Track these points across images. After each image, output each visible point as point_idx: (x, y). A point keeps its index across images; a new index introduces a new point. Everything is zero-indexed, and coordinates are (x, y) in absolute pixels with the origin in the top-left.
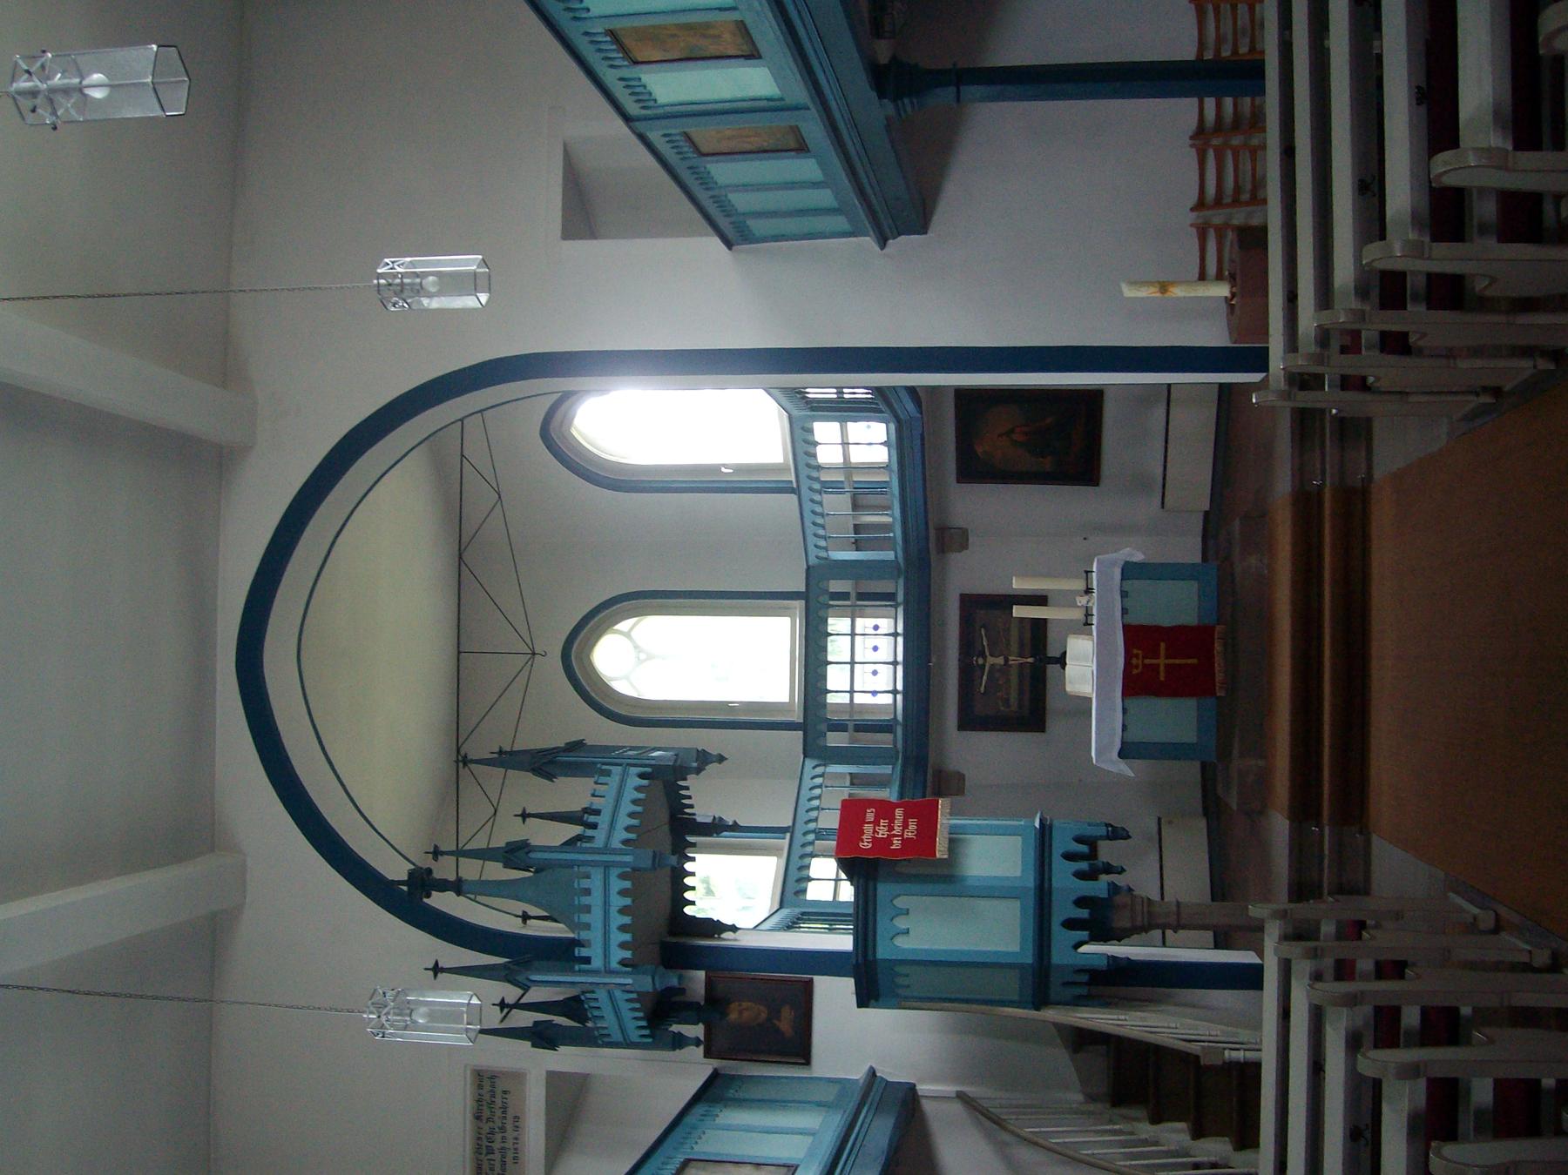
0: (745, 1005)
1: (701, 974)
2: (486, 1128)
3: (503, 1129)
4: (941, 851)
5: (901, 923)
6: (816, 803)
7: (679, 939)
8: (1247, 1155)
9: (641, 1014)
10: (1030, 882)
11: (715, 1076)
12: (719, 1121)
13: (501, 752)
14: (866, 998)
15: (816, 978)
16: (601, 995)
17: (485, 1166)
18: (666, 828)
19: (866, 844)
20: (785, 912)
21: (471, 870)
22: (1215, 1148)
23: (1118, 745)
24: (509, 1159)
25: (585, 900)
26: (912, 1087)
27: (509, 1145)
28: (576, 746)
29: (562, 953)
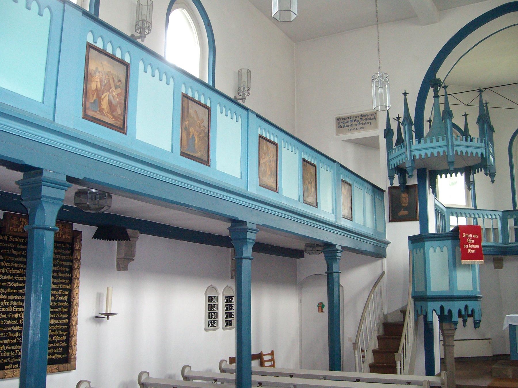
0: (408, 199)
1: (416, 183)
2: (359, 119)
3: (359, 124)
4: (464, 262)
5: (438, 249)
6: (486, 217)
7: (429, 175)
8: (368, 368)
9: (398, 164)
10: (456, 294)
11: (383, 191)
12: (366, 194)
13: (487, 103)
14: (413, 240)
15: (418, 222)
16: (403, 150)
17: (346, 121)
18: (467, 165)
19: (464, 235)
20: (445, 209)
21: (442, 100)
22: (370, 358)
23: (514, 324)
24: (350, 128)
25: (434, 140)
26: (384, 256)
27: (354, 127)
28: (491, 129)
29: (420, 135)
